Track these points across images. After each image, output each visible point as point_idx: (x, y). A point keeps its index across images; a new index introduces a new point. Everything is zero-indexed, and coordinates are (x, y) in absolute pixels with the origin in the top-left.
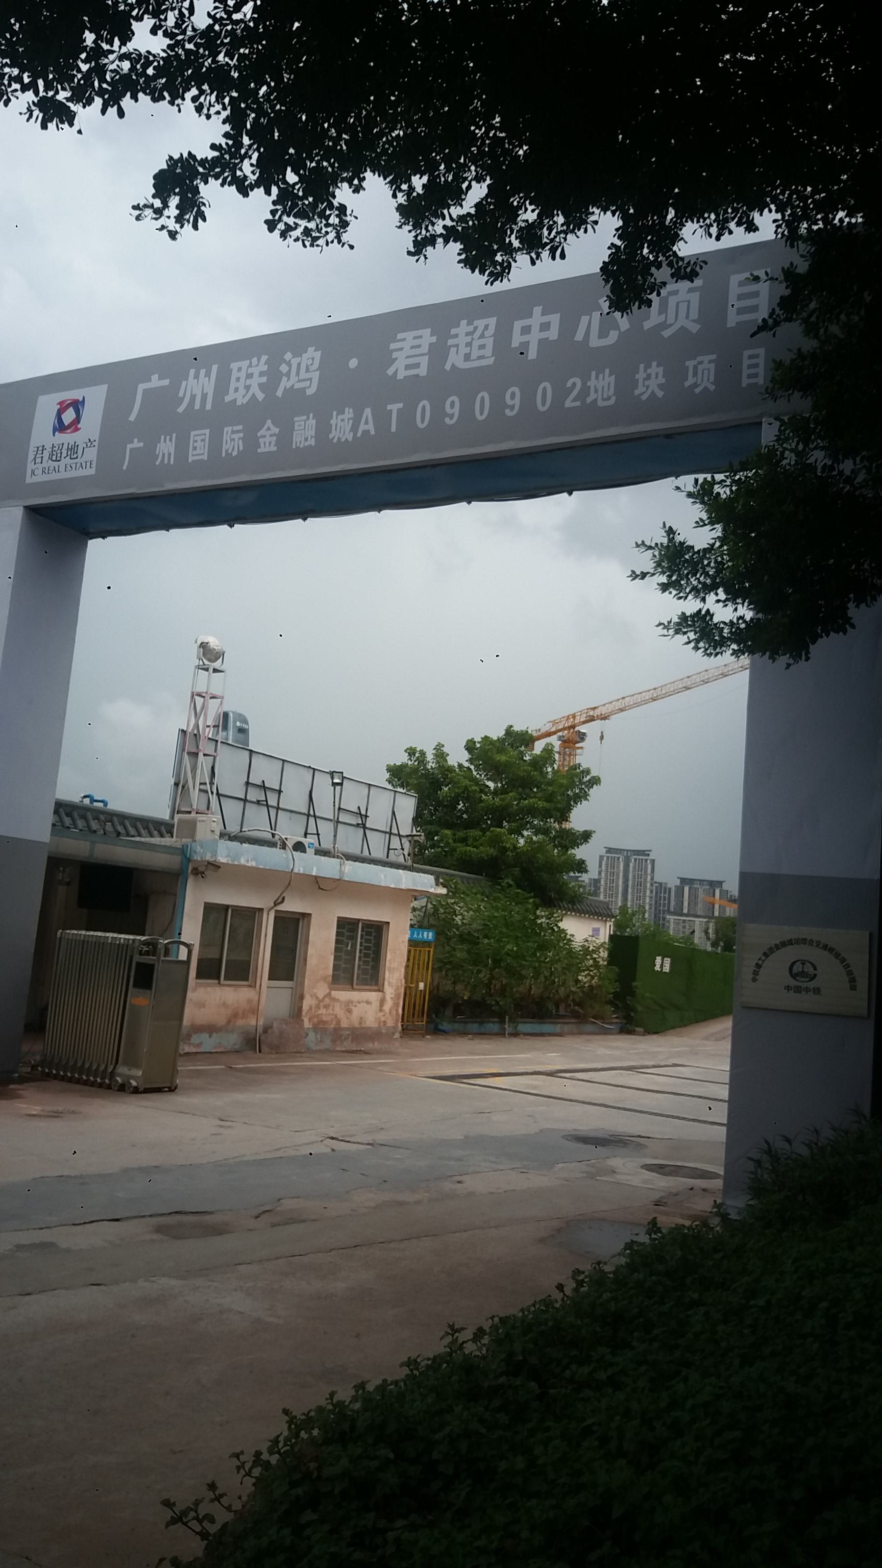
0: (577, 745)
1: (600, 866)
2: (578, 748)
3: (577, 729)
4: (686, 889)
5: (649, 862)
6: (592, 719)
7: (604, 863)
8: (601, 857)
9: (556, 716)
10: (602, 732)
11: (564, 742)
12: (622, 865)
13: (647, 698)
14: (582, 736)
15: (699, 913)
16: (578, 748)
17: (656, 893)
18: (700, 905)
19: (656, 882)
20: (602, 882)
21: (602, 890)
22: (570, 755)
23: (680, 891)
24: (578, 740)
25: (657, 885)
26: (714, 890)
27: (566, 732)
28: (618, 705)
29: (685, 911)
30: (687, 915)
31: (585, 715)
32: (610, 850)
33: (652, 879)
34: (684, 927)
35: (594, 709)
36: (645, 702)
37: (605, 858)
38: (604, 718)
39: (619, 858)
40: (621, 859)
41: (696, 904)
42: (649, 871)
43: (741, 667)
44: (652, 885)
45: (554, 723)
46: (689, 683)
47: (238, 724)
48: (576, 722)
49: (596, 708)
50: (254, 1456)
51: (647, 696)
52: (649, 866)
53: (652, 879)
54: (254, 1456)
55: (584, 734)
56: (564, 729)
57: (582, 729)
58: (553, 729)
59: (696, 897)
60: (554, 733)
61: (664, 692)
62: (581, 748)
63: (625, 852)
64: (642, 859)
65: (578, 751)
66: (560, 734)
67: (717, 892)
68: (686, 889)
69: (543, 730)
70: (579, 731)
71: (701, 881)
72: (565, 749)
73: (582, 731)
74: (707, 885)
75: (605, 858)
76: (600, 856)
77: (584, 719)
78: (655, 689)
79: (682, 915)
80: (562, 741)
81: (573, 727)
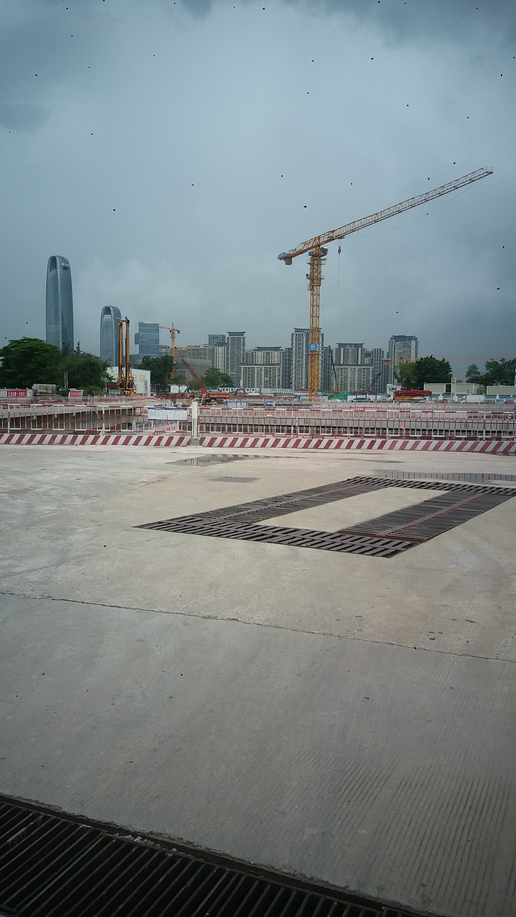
0: (322, 258)
1: (292, 340)
2: (323, 260)
3: (321, 247)
4: (342, 350)
5: (320, 335)
6: (331, 239)
7: (294, 338)
8: (292, 335)
9: (307, 239)
10: (340, 247)
11: (313, 256)
12: (305, 338)
13: (371, 221)
14: (325, 252)
15: (350, 363)
16: (323, 260)
17: (325, 353)
18: (350, 359)
19: (324, 347)
20: (294, 350)
21: (294, 354)
22: (317, 265)
23: (338, 351)
24: (322, 254)
25: (325, 349)
26: (358, 349)
27: (314, 249)
28: (349, 228)
29: (342, 363)
30: (343, 365)
31: (327, 237)
32: (297, 330)
33: (322, 345)
34: (342, 372)
35: (333, 232)
36: (370, 224)
37: (295, 335)
38: (341, 237)
39: (303, 334)
40: (304, 335)
41: (348, 358)
42: (321, 341)
43: (439, 194)
44: (322, 349)
45: (305, 244)
46: (400, 208)
47: (63, 264)
48: (320, 242)
49: (334, 231)
50: (393, 901)
51: (370, 219)
52: (321, 338)
53: (322, 345)
54: (393, 901)
55: (326, 250)
56: (313, 247)
57: (325, 246)
58: (305, 248)
59: (348, 354)
60: (306, 251)
61: (382, 216)
62: (325, 259)
63: (306, 331)
64: (300, 334)
65: (323, 262)
66: (311, 251)
67: (360, 350)
68: (342, 350)
69: (298, 249)
70: (323, 248)
71: (350, 345)
72: (314, 260)
73: (324, 248)
74: (354, 347)
75: (295, 335)
76: (292, 334)
77: (326, 239)
78: (376, 214)
79: (340, 365)
80: (312, 256)
81: (319, 246)
